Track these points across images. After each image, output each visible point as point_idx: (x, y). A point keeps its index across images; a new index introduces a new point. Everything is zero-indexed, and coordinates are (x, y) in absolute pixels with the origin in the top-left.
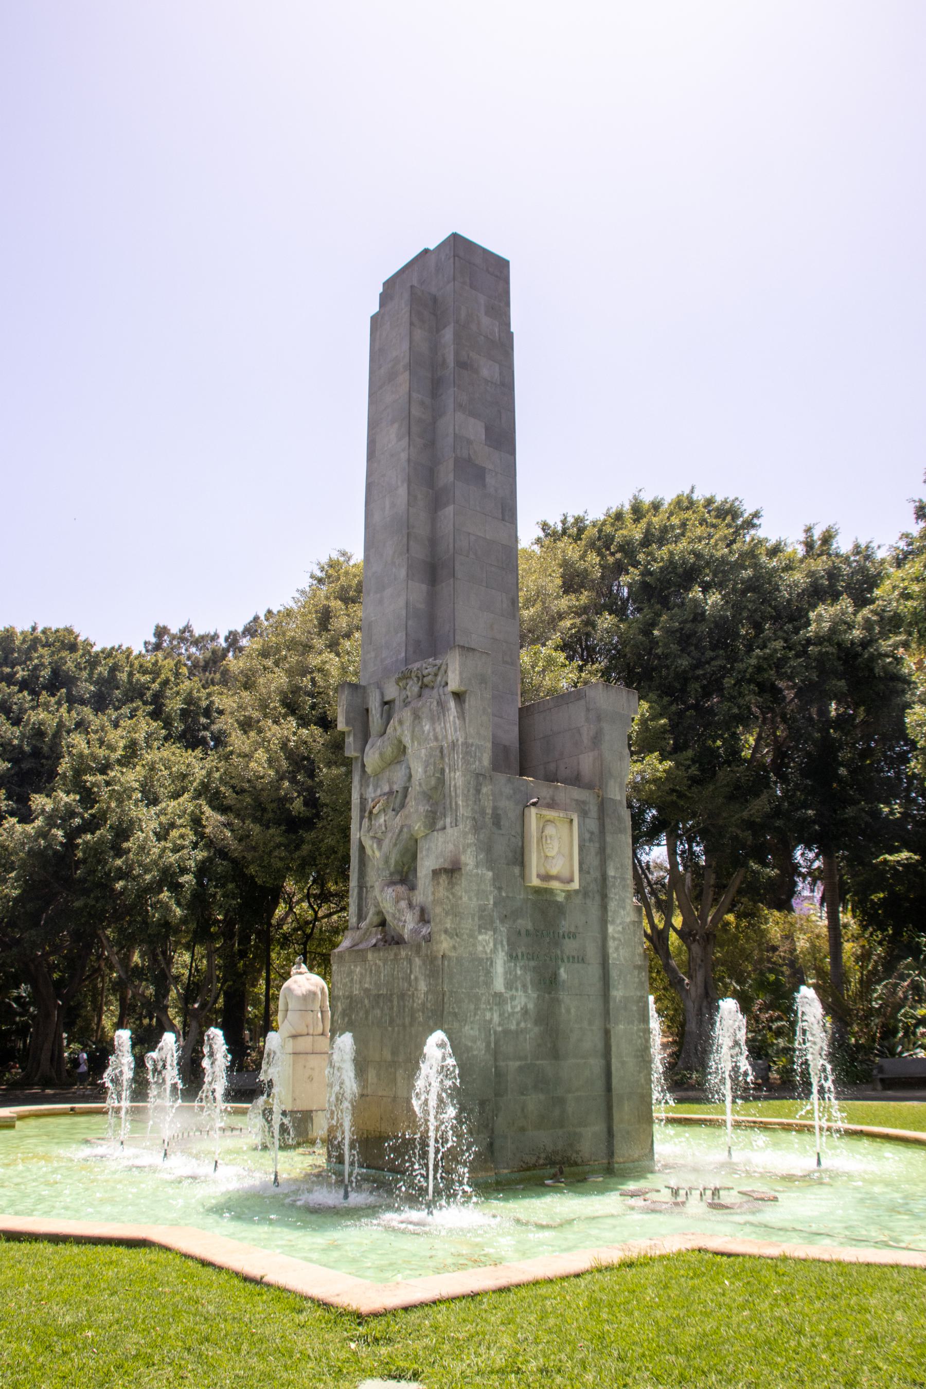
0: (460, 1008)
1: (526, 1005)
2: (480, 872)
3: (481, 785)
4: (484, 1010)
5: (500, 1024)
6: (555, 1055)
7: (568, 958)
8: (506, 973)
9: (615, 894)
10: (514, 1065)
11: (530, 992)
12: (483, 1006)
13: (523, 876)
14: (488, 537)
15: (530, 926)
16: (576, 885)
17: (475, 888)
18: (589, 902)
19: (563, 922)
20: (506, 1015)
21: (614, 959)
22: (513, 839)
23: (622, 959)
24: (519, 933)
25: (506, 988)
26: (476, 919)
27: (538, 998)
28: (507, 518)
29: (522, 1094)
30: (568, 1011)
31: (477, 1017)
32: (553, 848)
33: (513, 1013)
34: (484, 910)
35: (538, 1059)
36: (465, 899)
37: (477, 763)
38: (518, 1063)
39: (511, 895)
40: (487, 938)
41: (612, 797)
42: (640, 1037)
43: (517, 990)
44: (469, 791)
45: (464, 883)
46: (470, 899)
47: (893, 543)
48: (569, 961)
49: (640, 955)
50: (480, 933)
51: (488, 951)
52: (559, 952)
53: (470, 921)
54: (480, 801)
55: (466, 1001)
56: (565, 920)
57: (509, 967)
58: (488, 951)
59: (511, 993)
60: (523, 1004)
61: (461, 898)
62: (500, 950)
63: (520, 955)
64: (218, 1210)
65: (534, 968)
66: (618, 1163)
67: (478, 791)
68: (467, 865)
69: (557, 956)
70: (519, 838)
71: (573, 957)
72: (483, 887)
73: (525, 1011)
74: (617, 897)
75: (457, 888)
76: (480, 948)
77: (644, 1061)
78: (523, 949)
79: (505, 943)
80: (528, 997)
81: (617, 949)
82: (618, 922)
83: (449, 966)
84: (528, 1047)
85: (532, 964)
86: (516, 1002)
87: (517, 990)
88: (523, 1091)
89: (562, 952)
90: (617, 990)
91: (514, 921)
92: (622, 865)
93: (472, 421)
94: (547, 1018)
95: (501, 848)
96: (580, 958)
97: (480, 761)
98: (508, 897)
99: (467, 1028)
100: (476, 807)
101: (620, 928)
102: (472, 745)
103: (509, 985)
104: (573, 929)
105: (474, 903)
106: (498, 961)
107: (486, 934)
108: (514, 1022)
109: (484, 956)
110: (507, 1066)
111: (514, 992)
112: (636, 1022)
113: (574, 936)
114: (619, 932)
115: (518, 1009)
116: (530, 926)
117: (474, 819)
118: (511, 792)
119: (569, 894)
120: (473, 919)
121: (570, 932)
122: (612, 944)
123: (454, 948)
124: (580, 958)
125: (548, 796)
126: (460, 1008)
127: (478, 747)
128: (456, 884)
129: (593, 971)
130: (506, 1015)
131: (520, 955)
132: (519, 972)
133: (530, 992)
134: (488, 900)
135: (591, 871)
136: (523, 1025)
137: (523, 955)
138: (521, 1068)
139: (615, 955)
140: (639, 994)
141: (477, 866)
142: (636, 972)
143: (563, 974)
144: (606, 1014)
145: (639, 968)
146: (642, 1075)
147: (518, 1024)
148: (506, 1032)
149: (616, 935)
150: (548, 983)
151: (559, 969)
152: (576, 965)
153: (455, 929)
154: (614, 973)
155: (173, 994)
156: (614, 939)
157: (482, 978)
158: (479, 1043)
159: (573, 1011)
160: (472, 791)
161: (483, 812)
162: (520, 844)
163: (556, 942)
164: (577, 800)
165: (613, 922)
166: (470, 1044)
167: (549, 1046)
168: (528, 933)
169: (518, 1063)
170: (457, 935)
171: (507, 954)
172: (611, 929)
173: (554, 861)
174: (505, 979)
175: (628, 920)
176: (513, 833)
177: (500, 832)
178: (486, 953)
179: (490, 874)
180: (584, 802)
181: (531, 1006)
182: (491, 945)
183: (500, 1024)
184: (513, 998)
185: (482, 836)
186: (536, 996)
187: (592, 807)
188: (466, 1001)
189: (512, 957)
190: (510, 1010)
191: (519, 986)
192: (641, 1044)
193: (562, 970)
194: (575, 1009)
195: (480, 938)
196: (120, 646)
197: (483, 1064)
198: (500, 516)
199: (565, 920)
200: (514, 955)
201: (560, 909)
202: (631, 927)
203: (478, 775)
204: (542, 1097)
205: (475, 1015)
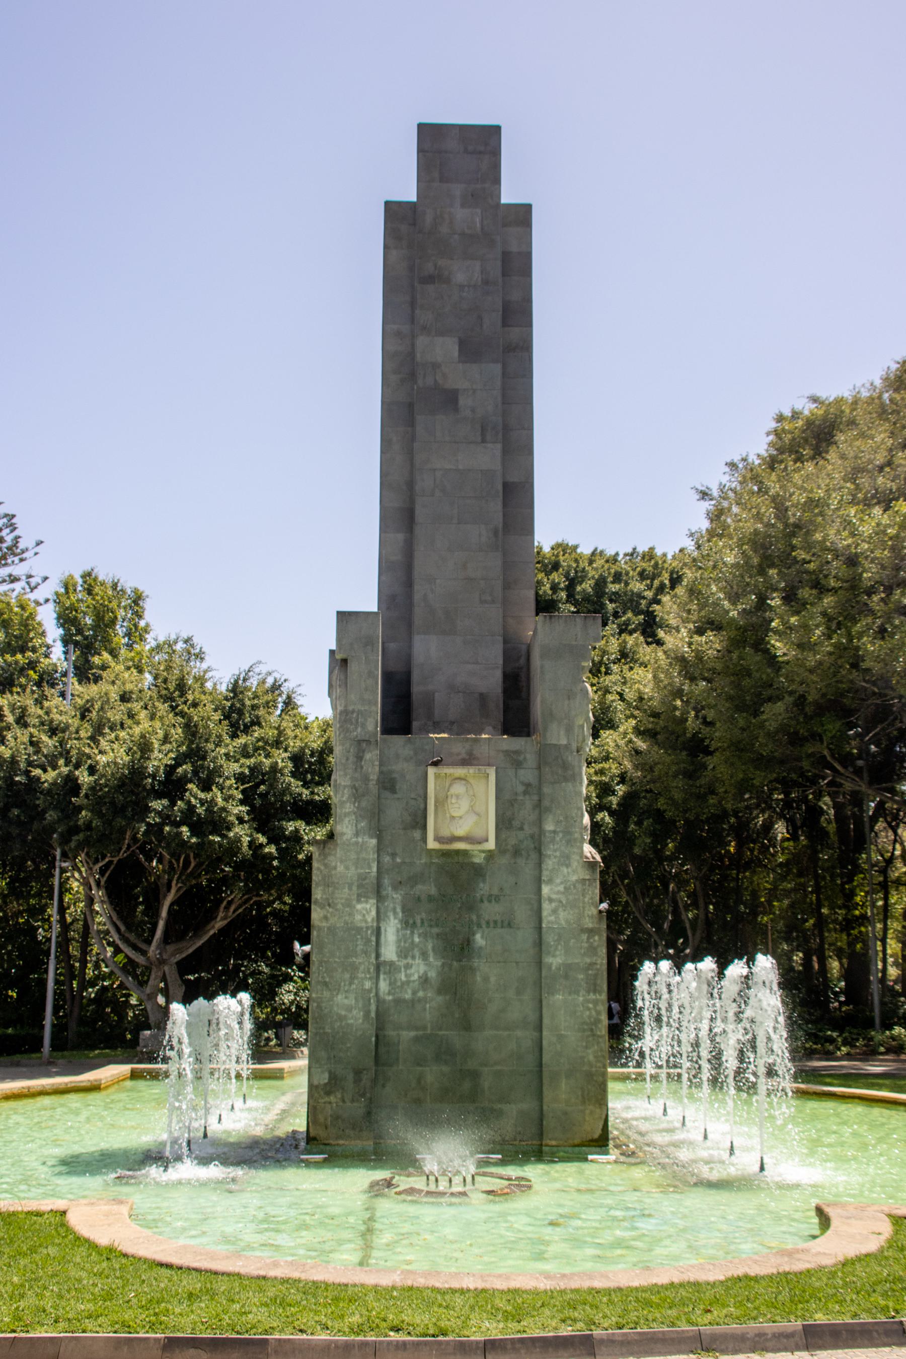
0: (331, 977)
1: (425, 973)
2: (360, 840)
3: (364, 751)
4: (362, 979)
5: (389, 993)
6: (467, 1026)
7: (488, 923)
8: (399, 941)
9: (555, 851)
10: (407, 1035)
11: (431, 959)
12: (361, 975)
13: (424, 839)
14: (461, 467)
15: (433, 891)
16: (491, 845)
17: (353, 856)
18: (521, 861)
19: (481, 885)
20: (399, 984)
21: (549, 922)
22: (413, 802)
23: (563, 922)
24: (419, 899)
25: (399, 956)
26: (354, 888)
27: (443, 965)
28: (488, 438)
29: (419, 1065)
30: (486, 979)
31: (354, 986)
32: (459, 807)
33: (408, 982)
34: (365, 879)
35: (440, 1029)
36: (341, 868)
37: (359, 730)
38: (413, 1034)
39: (407, 860)
40: (368, 906)
41: (554, 742)
42: (589, 1009)
43: (413, 958)
44: (347, 759)
45: (339, 852)
46: (347, 868)
47: (858, 384)
48: (488, 927)
49: (592, 917)
50: (359, 901)
51: (369, 920)
52: (474, 917)
53: (346, 890)
54: (362, 767)
55: (340, 970)
56: (484, 881)
57: (404, 935)
58: (369, 920)
59: (405, 961)
60: (422, 972)
61: (335, 868)
62: (392, 918)
63: (419, 922)
64: (889, 1216)
65: (438, 935)
66: (547, 1145)
67: (359, 758)
68: (343, 834)
69: (471, 921)
70: (421, 800)
71: (495, 922)
72: (364, 855)
73: (425, 981)
74: (558, 854)
75: (331, 858)
76: (358, 917)
77: (594, 1035)
78: (424, 915)
79: (399, 910)
80: (429, 965)
81: (555, 911)
82: (558, 881)
83: (318, 936)
84: (428, 1016)
85: (435, 930)
86: (412, 971)
87: (413, 958)
88: (420, 1061)
89: (479, 917)
90: (554, 956)
91: (412, 887)
92: (566, 818)
93: (439, 340)
94: (456, 988)
95: (395, 811)
96: (506, 924)
97: (363, 726)
98: (403, 863)
99: (340, 997)
100: (357, 775)
101: (561, 888)
102: (353, 712)
103: (403, 953)
104: (495, 891)
105: (352, 872)
106: (388, 929)
107: (367, 902)
108: (410, 991)
109: (364, 925)
110: (398, 1035)
111: (410, 961)
112: (582, 992)
113: (497, 899)
114: (558, 892)
115: (416, 977)
116: (433, 891)
117: (354, 787)
118: (412, 753)
119: (490, 855)
120: (350, 889)
121: (491, 895)
122: (547, 907)
123: (326, 918)
124: (492, 925)
125: (464, 751)
126: (331, 977)
127: (359, 712)
128: (330, 854)
129: (524, 936)
130: (399, 984)
131: (419, 922)
132: (417, 940)
133: (431, 959)
134: (370, 867)
135: (526, 827)
136: (421, 994)
137: (422, 922)
138: (417, 1039)
139: (552, 918)
140: (588, 960)
141: (357, 834)
142: (585, 937)
143: (479, 939)
144: (539, 984)
145: (591, 932)
146: (590, 1051)
147: (414, 993)
148: (398, 1002)
149: (554, 896)
150: (457, 949)
151: (474, 935)
152: (499, 930)
153: (327, 899)
154: (549, 939)
155: (89, 965)
156: (551, 900)
157: (360, 948)
158: (355, 1012)
159: (493, 979)
160: (352, 759)
161: (366, 779)
162: (422, 806)
163: (471, 906)
164: (507, 751)
165: (550, 881)
166: (343, 1013)
167: (457, 1016)
168: (430, 899)
169: (413, 1034)
170: (329, 905)
171: (401, 921)
172: (546, 890)
173: (461, 822)
174: (398, 947)
175: (574, 878)
176: (413, 796)
177: (396, 796)
178: (366, 922)
179: (374, 842)
180: (517, 752)
181: (432, 974)
182: (374, 913)
183: (389, 993)
184: (408, 967)
185: (364, 804)
186: (439, 964)
187: (528, 756)
188: (340, 970)
189: (407, 924)
190: (403, 978)
191: (417, 954)
192: (590, 1017)
193: (478, 937)
194: (488, 975)
195: (359, 907)
196: (576, 547)
197: (359, 1033)
198: (479, 439)
199: (484, 881)
200: (411, 922)
201: (478, 872)
202: (579, 886)
203: (360, 742)
204: (445, 1069)
205: (350, 984)
